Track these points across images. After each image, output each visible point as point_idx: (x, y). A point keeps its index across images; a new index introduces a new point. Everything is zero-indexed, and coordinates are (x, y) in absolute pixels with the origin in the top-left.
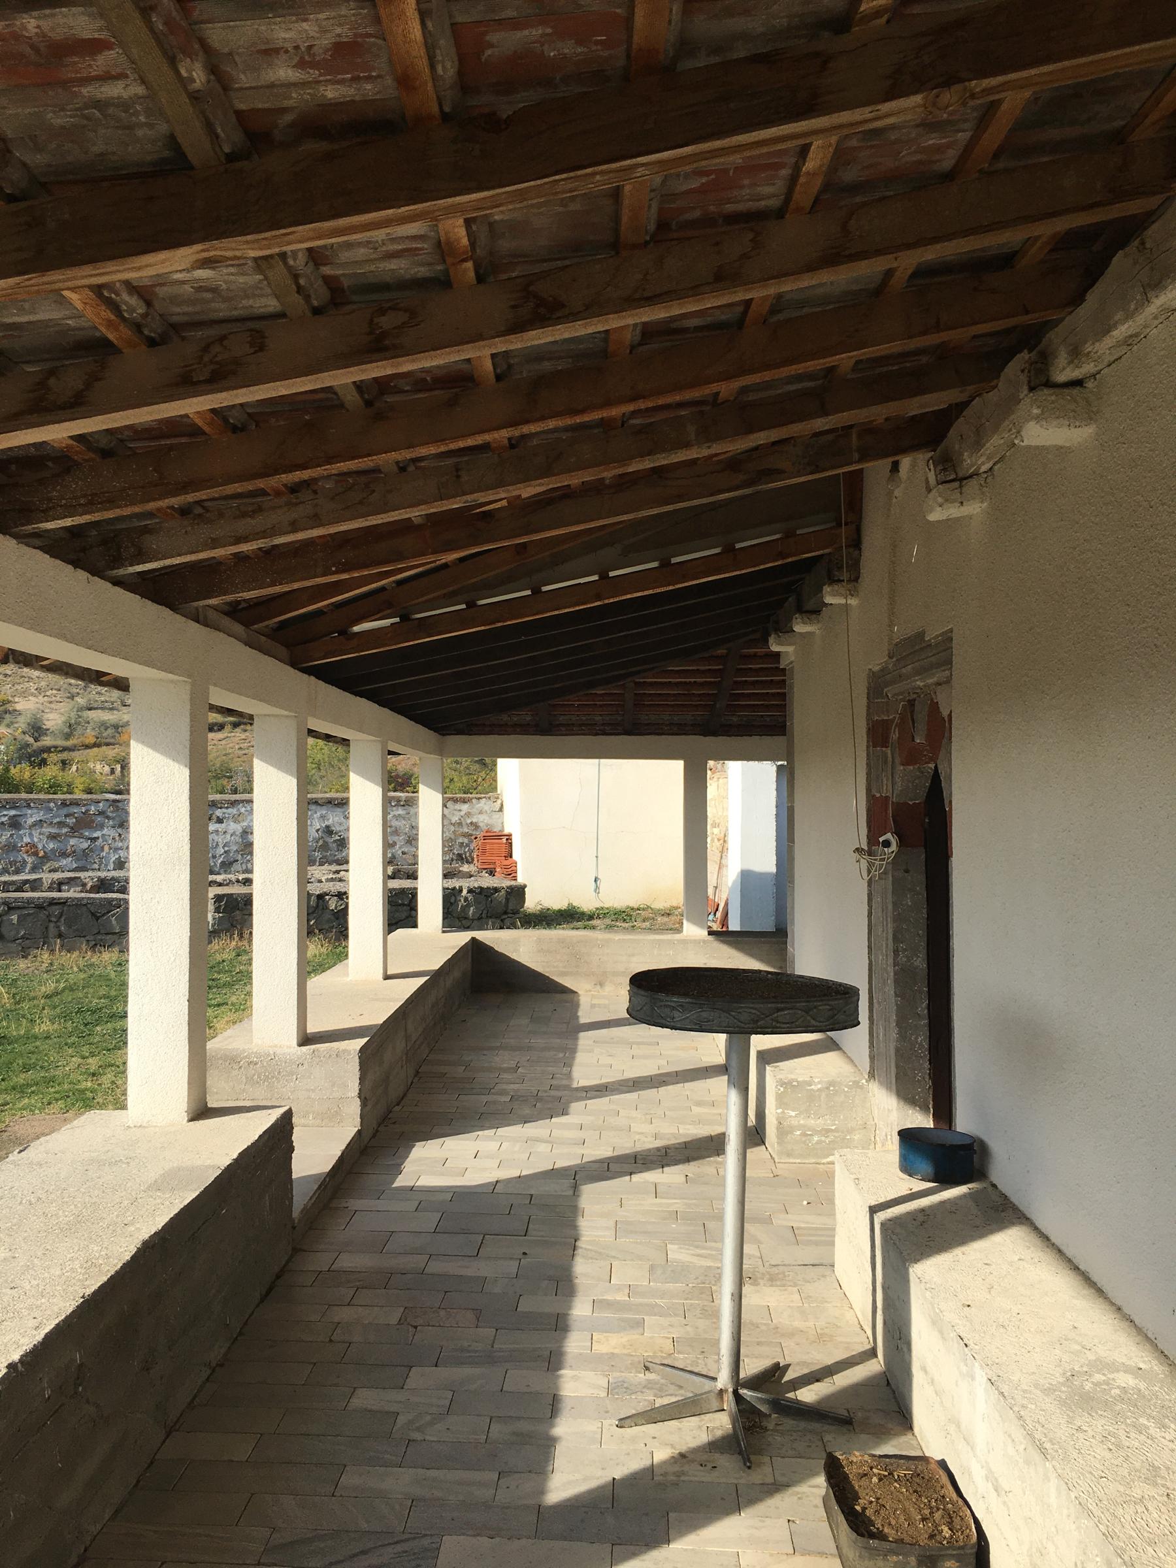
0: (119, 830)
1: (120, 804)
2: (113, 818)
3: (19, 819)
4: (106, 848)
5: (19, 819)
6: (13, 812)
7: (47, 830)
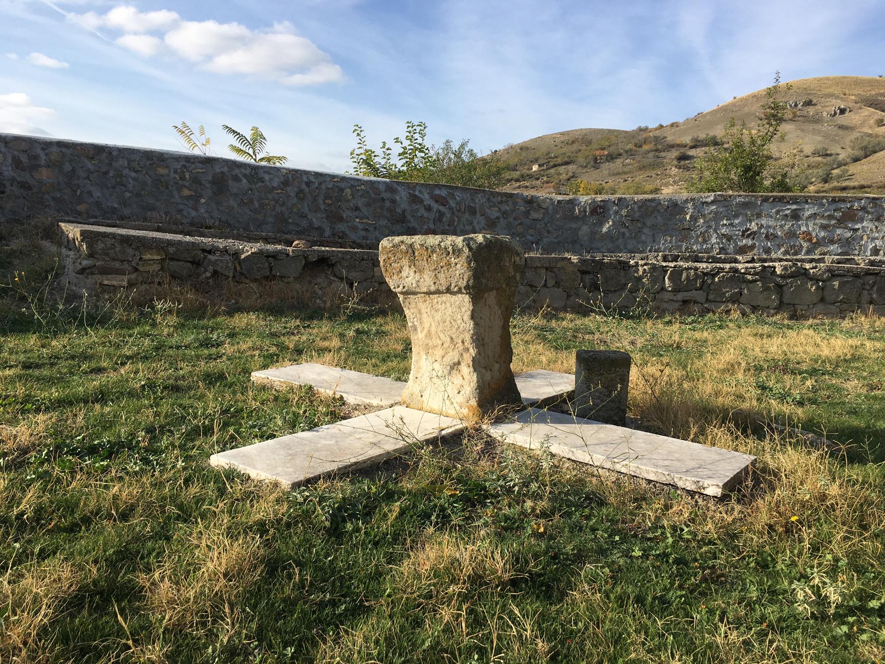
0: (876, 223)
1: (878, 202)
2: (872, 213)
3: (798, 212)
4: (865, 238)
5: (798, 212)
6: (794, 207)
7: (819, 221)
